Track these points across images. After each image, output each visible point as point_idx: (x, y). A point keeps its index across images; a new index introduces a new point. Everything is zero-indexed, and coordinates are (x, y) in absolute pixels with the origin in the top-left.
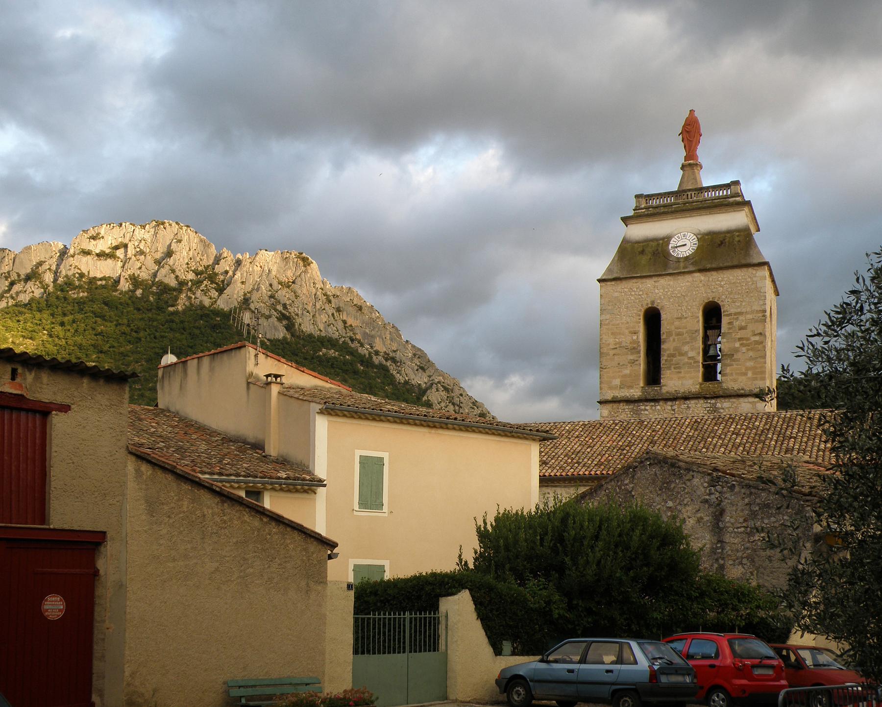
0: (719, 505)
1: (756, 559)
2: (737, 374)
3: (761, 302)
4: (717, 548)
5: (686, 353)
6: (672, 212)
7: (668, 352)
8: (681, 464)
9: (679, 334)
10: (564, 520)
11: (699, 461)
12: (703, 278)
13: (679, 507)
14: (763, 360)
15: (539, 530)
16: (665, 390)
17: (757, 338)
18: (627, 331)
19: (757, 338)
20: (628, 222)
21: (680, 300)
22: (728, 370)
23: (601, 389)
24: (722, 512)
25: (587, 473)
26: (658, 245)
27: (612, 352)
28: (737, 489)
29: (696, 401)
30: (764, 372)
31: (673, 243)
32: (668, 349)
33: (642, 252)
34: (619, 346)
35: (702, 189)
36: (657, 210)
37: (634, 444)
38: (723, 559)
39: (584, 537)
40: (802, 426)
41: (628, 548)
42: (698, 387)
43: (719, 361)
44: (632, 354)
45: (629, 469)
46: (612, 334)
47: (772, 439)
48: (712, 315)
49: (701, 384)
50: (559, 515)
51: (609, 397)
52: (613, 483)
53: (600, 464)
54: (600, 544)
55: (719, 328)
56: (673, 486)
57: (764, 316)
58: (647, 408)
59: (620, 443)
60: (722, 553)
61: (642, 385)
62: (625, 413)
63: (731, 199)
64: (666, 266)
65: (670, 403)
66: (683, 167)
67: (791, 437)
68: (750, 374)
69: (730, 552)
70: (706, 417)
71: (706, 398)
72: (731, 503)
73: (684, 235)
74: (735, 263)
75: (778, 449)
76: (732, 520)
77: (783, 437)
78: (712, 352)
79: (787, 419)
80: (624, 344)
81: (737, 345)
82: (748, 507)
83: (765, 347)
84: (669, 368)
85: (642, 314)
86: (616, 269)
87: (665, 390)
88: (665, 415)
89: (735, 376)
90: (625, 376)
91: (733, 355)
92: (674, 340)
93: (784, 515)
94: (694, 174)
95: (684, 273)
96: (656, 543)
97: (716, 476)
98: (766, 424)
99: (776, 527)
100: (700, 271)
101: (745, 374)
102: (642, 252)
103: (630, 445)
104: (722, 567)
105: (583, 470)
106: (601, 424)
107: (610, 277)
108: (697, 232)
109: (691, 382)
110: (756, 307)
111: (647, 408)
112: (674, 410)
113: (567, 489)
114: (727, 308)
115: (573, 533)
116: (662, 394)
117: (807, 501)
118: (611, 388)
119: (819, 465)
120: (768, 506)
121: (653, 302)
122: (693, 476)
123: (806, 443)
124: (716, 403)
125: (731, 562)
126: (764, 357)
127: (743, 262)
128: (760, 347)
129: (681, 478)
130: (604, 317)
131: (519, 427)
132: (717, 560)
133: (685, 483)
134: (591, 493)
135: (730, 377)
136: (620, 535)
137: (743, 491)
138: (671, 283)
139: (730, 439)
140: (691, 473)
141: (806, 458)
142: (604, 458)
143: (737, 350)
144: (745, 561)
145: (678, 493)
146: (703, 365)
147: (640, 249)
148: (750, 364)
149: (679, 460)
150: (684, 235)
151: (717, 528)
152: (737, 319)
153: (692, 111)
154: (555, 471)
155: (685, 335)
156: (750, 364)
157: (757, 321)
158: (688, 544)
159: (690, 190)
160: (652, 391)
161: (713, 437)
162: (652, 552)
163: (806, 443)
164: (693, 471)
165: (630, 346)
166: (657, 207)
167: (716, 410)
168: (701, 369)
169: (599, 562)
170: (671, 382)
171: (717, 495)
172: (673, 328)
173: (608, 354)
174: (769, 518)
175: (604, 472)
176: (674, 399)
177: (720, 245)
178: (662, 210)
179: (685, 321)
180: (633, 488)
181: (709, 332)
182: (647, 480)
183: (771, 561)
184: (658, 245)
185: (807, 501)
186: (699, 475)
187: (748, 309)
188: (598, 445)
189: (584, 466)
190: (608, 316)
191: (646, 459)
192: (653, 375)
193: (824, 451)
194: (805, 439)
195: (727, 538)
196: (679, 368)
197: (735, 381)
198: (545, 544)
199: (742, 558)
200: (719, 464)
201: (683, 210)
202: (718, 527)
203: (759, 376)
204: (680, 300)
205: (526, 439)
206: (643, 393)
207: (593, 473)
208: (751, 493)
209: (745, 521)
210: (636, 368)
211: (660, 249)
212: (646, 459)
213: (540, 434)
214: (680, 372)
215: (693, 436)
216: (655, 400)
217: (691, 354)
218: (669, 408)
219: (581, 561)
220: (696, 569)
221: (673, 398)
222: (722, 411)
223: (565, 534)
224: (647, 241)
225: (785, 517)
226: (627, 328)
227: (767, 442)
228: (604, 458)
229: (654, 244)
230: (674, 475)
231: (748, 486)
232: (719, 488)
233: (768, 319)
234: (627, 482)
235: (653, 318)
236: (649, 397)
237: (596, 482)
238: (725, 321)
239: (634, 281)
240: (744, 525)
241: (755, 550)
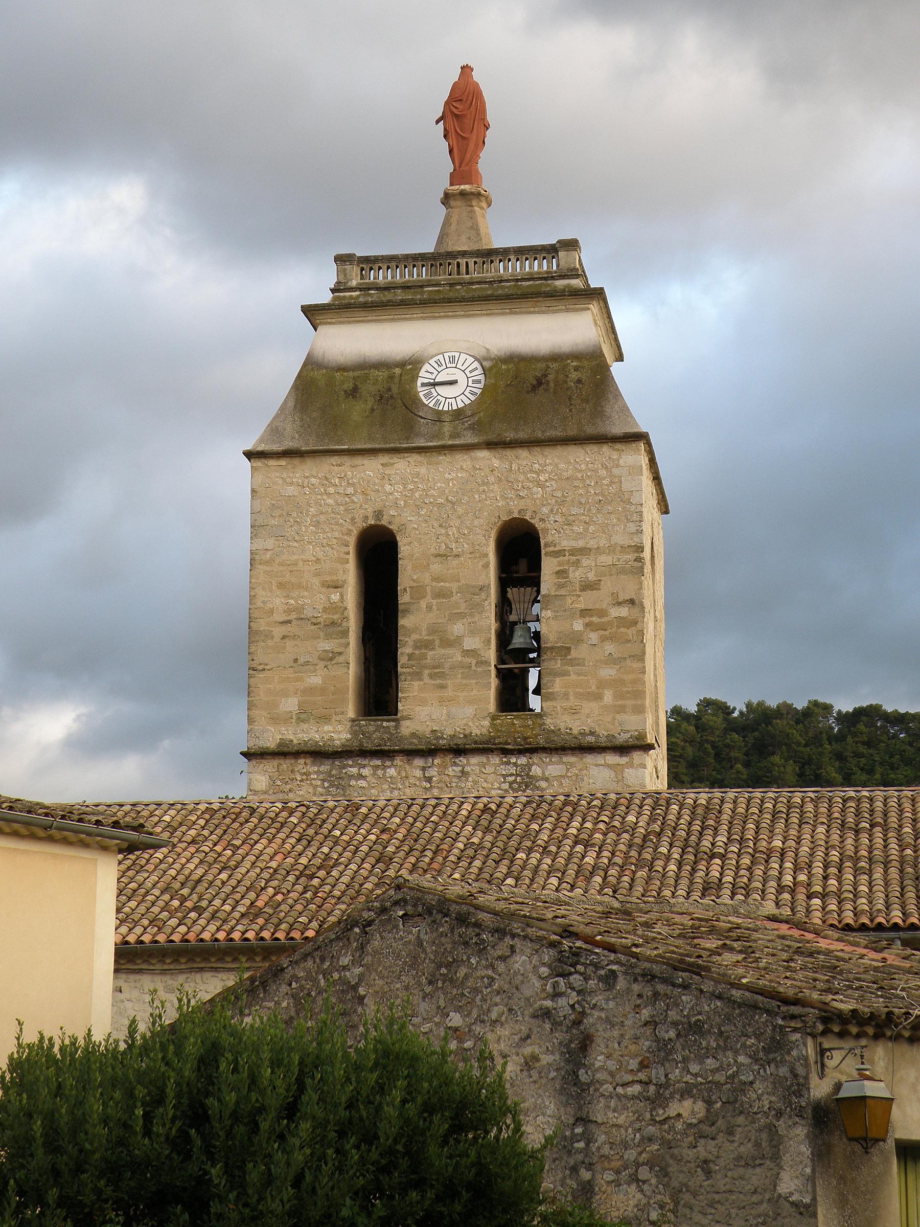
0: (577, 1023)
1: (673, 1168)
2: (578, 696)
3: (632, 527)
4: (574, 1138)
5: (458, 640)
6: (424, 303)
7: (415, 637)
8: (482, 916)
9: (441, 594)
10: (209, 1058)
11: (526, 911)
12: (496, 463)
13: (478, 1029)
14: (636, 665)
15: (140, 1092)
16: (407, 728)
17: (624, 612)
18: (316, 581)
19: (624, 612)
20: (319, 319)
21: (448, 513)
22: (557, 686)
23: (251, 721)
24: (586, 1043)
25: (221, 936)
26: (391, 377)
27: (278, 631)
28: (621, 983)
29: (483, 759)
30: (639, 694)
31: (425, 375)
32: (416, 629)
33: (354, 393)
34: (296, 617)
35: (490, 255)
36: (388, 296)
37: (337, 864)
38: (590, 1167)
39: (262, 1109)
40: (737, 829)
41: (369, 1138)
42: (487, 723)
43: (535, 662)
44: (328, 637)
45: (354, 929)
46: (281, 585)
47: (668, 858)
48: (519, 552)
49: (494, 718)
50: (192, 1048)
51: (270, 741)
52: (310, 963)
53: (252, 913)
54: (305, 1126)
55: (535, 583)
56: (462, 972)
57: (639, 560)
58: (366, 772)
59: (304, 860)
60: (586, 1151)
61: (351, 713)
62: (308, 784)
63: (554, 279)
64: (409, 428)
65: (419, 762)
66: (447, 198)
67: (713, 856)
68: (608, 696)
69: (606, 1150)
70: (509, 800)
71: (505, 752)
72: (607, 1020)
73: (452, 356)
74: (572, 432)
75: (684, 882)
76: (612, 1065)
77: (695, 855)
78: (518, 640)
79: (700, 811)
80: (309, 613)
81: (578, 625)
82: (648, 1031)
83: (641, 633)
84: (418, 676)
85: (352, 541)
86: (289, 428)
87: (407, 728)
88: (409, 792)
89: (572, 702)
90: (310, 691)
91: (569, 649)
92: (429, 608)
93: (736, 1053)
94: (472, 215)
95: (452, 448)
96: (440, 1124)
97: (570, 952)
98: (652, 819)
99: (718, 1084)
100: (490, 445)
101: (598, 697)
102: (354, 393)
103: (327, 865)
104: (587, 1189)
105: (212, 928)
106: (253, 811)
107: (275, 447)
108: (483, 353)
109: (469, 711)
110: (620, 539)
111: (366, 772)
112: (429, 780)
113: (167, 979)
114: (553, 536)
115: (231, 1098)
116: (401, 739)
117: (793, 1017)
118: (275, 720)
119: (801, 926)
120: (697, 1028)
121: (379, 514)
122: (512, 949)
123: (749, 869)
124: (529, 766)
125: (609, 1176)
126: (641, 657)
127: (590, 430)
128: (631, 632)
129: (481, 951)
130: (260, 544)
131: (67, 812)
132: (574, 1170)
133: (492, 966)
134: (252, 991)
135: (560, 703)
136: (350, 1106)
137: (636, 988)
138: (423, 470)
139: (570, 855)
140: (507, 939)
141: (769, 907)
142: (264, 898)
143: (578, 639)
144: (644, 1173)
145: (476, 991)
146: (498, 670)
147: (348, 386)
148: (608, 672)
149: (477, 907)
150: (452, 356)
151: (574, 1085)
152: (577, 564)
153: (466, 70)
154: (138, 930)
155: (456, 597)
156: (608, 672)
157: (622, 571)
158: (517, 1129)
159: (464, 254)
160: (377, 731)
161: (530, 850)
162: (433, 1149)
163: (749, 869)
164: (513, 936)
165: (324, 618)
166: (387, 288)
167: (527, 781)
168: (494, 682)
169: (297, 1182)
170: (425, 709)
171: (574, 997)
172: (426, 578)
173: (269, 636)
174: (701, 1060)
175: (266, 934)
176: (430, 752)
177: (534, 388)
178: (400, 295)
179: (455, 562)
180: (361, 977)
181: (512, 593)
182: (398, 956)
183: (708, 1173)
184: (391, 377)
185: (793, 1017)
186: (528, 947)
187: (603, 542)
188: (247, 864)
189: (213, 916)
190: (270, 543)
191: (396, 903)
192: (379, 692)
193: (793, 892)
194: (746, 861)
195: (600, 1112)
196: (442, 675)
197: (574, 712)
198: (158, 1129)
199: (638, 1165)
200: (574, 919)
201: (450, 301)
202: (576, 1082)
203: (629, 703)
204: (448, 513)
205: (85, 845)
206: (354, 734)
207: (236, 935)
208: (656, 994)
209: (643, 1066)
210: (339, 672)
211: (395, 389)
212: (396, 903)
213: (120, 833)
214: (443, 687)
215: (480, 846)
216: (383, 754)
217: (470, 643)
218: (418, 773)
219: (254, 1174)
220: (533, 1196)
221: (428, 750)
222: (543, 784)
223: (211, 1102)
224: (364, 369)
225: (741, 1059)
226: (317, 574)
227: (659, 865)
228: (264, 898)
229: (382, 375)
230: (466, 944)
231: (650, 977)
232: (576, 980)
233: (647, 568)
234: (345, 961)
235: (378, 554)
236: (369, 746)
237: (264, 961)
238: (548, 566)
239: (335, 460)
240: (642, 1076)
241: (668, 1145)
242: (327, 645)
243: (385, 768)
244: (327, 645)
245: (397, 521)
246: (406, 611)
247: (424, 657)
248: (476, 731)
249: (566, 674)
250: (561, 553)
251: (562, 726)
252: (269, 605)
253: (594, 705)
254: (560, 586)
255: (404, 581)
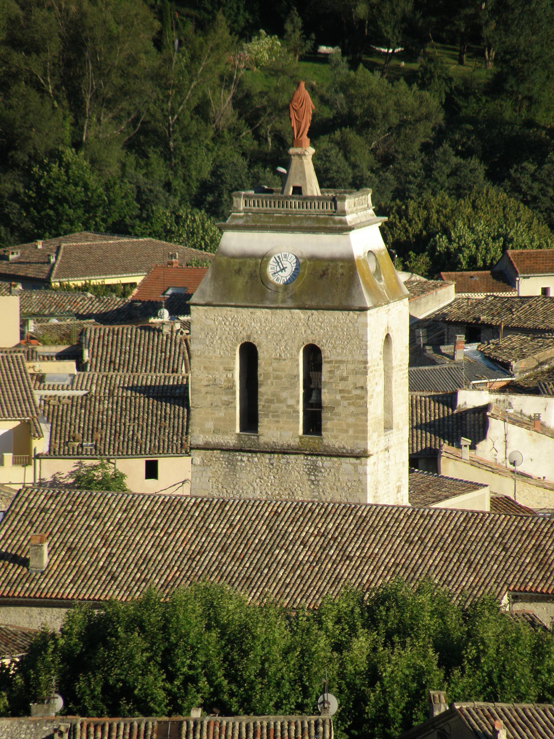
3: (363, 352)
5: (285, 400)
7: (266, 397)
9: (277, 377)
16: (263, 440)
17: (358, 392)
18: (221, 368)
26: (257, 264)
27: (204, 390)
32: (265, 394)
33: (238, 272)
42: (298, 440)
44: (226, 394)
48: (313, 356)
65: (267, 456)
68: (351, 432)
74: (336, 304)
81: (338, 397)
84: (266, 415)
89: (335, 433)
90: (218, 419)
92: (272, 383)
101: (346, 431)
102: (238, 272)
111: (245, 459)
114: (327, 353)
118: (203, 431)
121: (249, 337)
127: (345, 303)
128: (362, 402)
143: (338, 403)
147: (236, 267)
148: (351, 420)
155: (284, 380)
156: (351, 420)
160: (249, 438)
165: (223, 384)
170: (269, 431)
173: (200, 392)
179: (284, 363)
184: (257, 264)
192: (250, 420)
196: (278, 416)
197: (336, 437)
206: (239, 441)
214: (278, 422)
218: (267, 461)
221: (273, 451)
226: (222, 363)
229: (252, 262)
235: (249, 353)
242: (225, 398)
243: (252, 457)
244: (225, 398)
245: (257, 340)
246: (262, 384)
247: (269, 407)
248: (292, 443)
249: (332, 419)
250: (330, 362)
251: (331, 444)
252: (200, 377)
253: (345, 435)
254: (331, 378)
255: (260, 371)
